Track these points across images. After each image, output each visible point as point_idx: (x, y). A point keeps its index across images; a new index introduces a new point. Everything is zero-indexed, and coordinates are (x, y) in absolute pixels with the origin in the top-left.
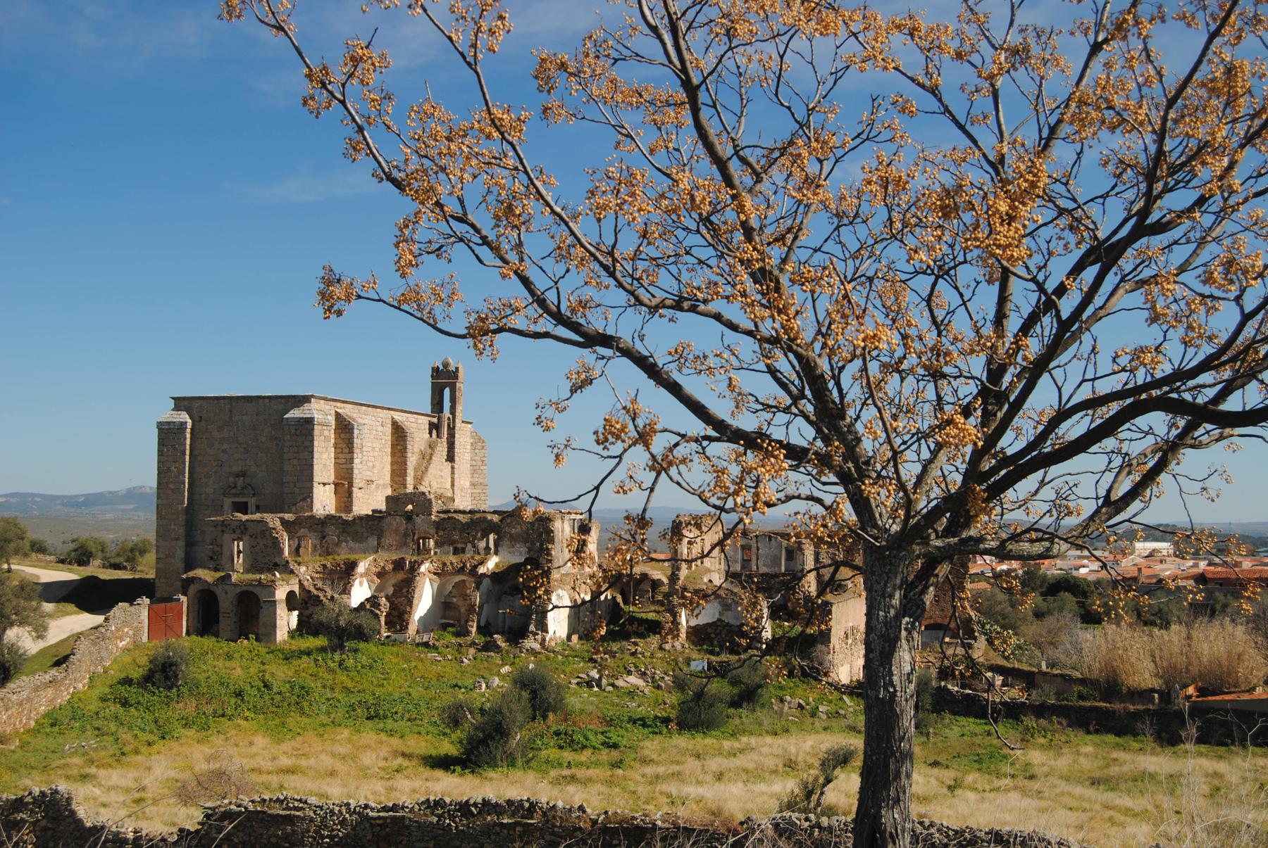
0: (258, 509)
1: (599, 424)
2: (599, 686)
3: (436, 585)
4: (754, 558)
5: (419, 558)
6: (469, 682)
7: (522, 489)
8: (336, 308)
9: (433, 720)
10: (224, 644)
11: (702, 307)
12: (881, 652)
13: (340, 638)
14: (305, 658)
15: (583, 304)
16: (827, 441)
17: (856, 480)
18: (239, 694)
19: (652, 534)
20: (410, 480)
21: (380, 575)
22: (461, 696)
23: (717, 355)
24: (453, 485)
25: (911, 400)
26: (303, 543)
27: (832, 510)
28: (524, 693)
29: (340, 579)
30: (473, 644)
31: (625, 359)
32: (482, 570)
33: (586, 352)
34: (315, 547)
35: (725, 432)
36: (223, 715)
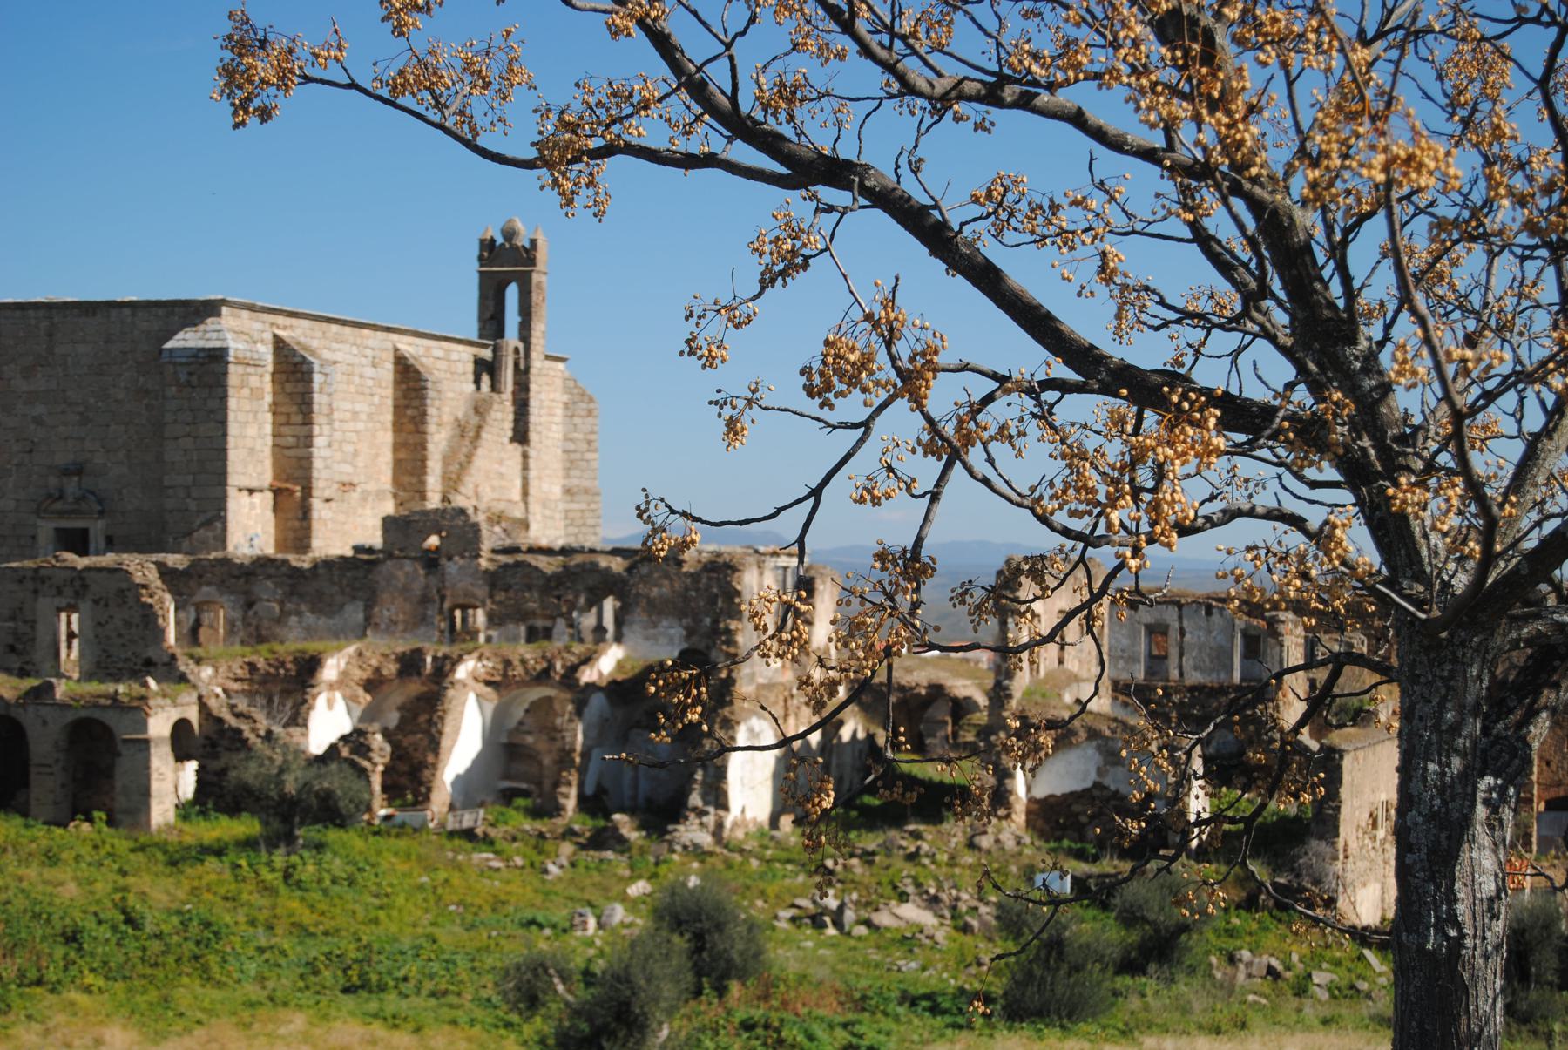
0: (111, 544)
1: (812, 353)
2: (838, 924)
3: (490, 708)
4: (1174, 652)
5: (454, 650)
6: (560, 915)
7: (655, 494)
8: (257, 102)
9: (484, 994)
10: (39, 831)
11: (1044, 98)
12: (1432, 851)
13: (287, 819)
14: (212, 862)
15: (789, 94)
16: (1317, 389)
17: (1379, 475)
18: (72, 937)
19: (934, 592)
20: (433, 482)
21: (370, 685)
22: (543, 946)
23: (1075, 203)
24: (525, 493)
25: (1509, 302)
26: (206, 618)
27: (1322, 538)
28: (676, 939)
29: (286, 693)
30: (569, 833)
31: (878, 213)
32: (587, 676)
33: (794, 196)
34: (231, 624)
35: (1093, 369)
36: (39, 982)
